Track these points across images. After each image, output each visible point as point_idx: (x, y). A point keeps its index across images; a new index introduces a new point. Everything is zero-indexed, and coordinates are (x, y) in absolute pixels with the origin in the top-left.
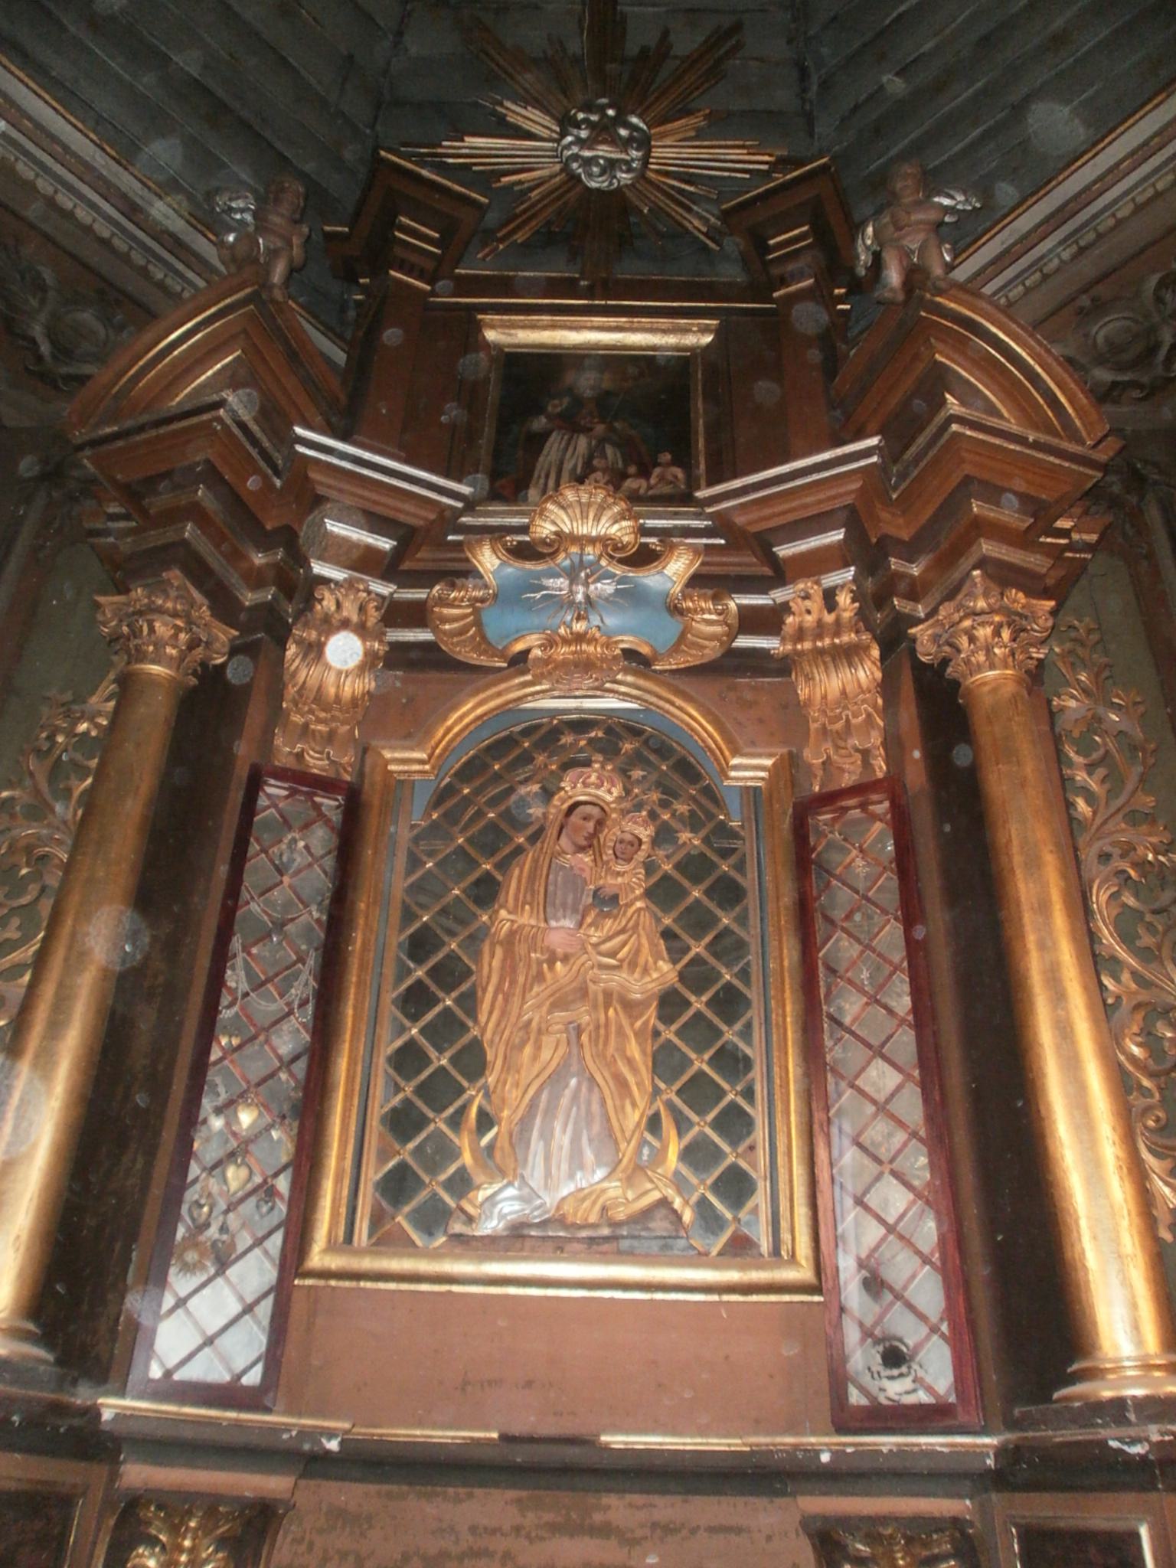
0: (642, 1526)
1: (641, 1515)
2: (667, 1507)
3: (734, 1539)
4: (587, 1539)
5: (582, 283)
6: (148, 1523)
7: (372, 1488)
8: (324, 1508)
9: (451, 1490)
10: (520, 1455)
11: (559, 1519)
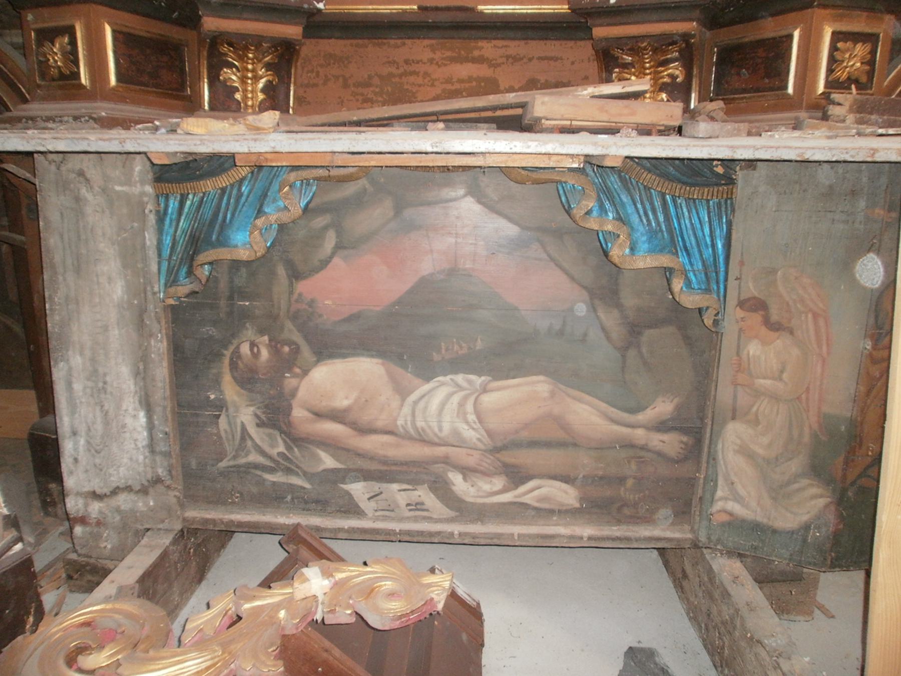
0: (501, 57)
1: (502, 52)
2: (516, 47)
3: (543, 55)
4: (470, 64)
5: (151, 504)
6: (226, 55)
7: (349, 42)
8: (322, 54)
9: (392, 42)
10: (431, 18)
11: (454, 54)
